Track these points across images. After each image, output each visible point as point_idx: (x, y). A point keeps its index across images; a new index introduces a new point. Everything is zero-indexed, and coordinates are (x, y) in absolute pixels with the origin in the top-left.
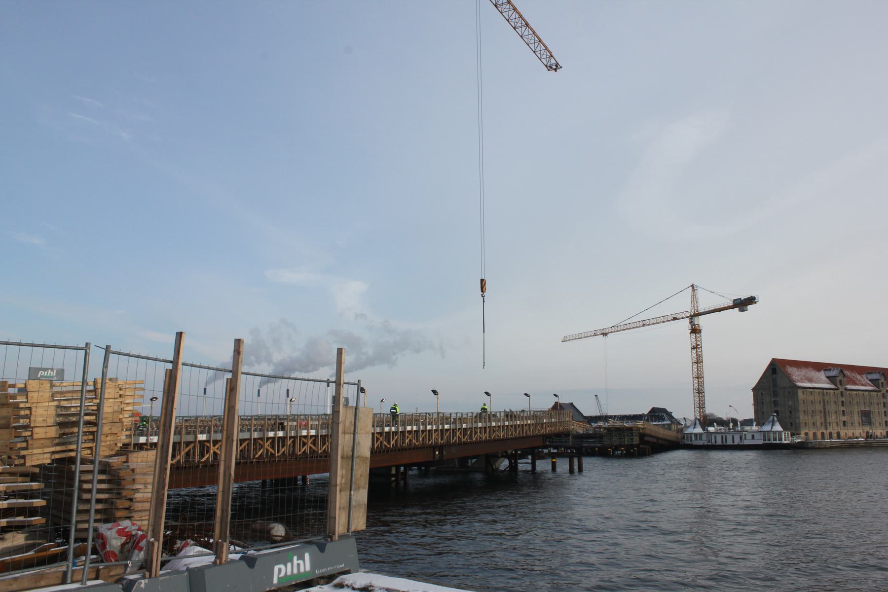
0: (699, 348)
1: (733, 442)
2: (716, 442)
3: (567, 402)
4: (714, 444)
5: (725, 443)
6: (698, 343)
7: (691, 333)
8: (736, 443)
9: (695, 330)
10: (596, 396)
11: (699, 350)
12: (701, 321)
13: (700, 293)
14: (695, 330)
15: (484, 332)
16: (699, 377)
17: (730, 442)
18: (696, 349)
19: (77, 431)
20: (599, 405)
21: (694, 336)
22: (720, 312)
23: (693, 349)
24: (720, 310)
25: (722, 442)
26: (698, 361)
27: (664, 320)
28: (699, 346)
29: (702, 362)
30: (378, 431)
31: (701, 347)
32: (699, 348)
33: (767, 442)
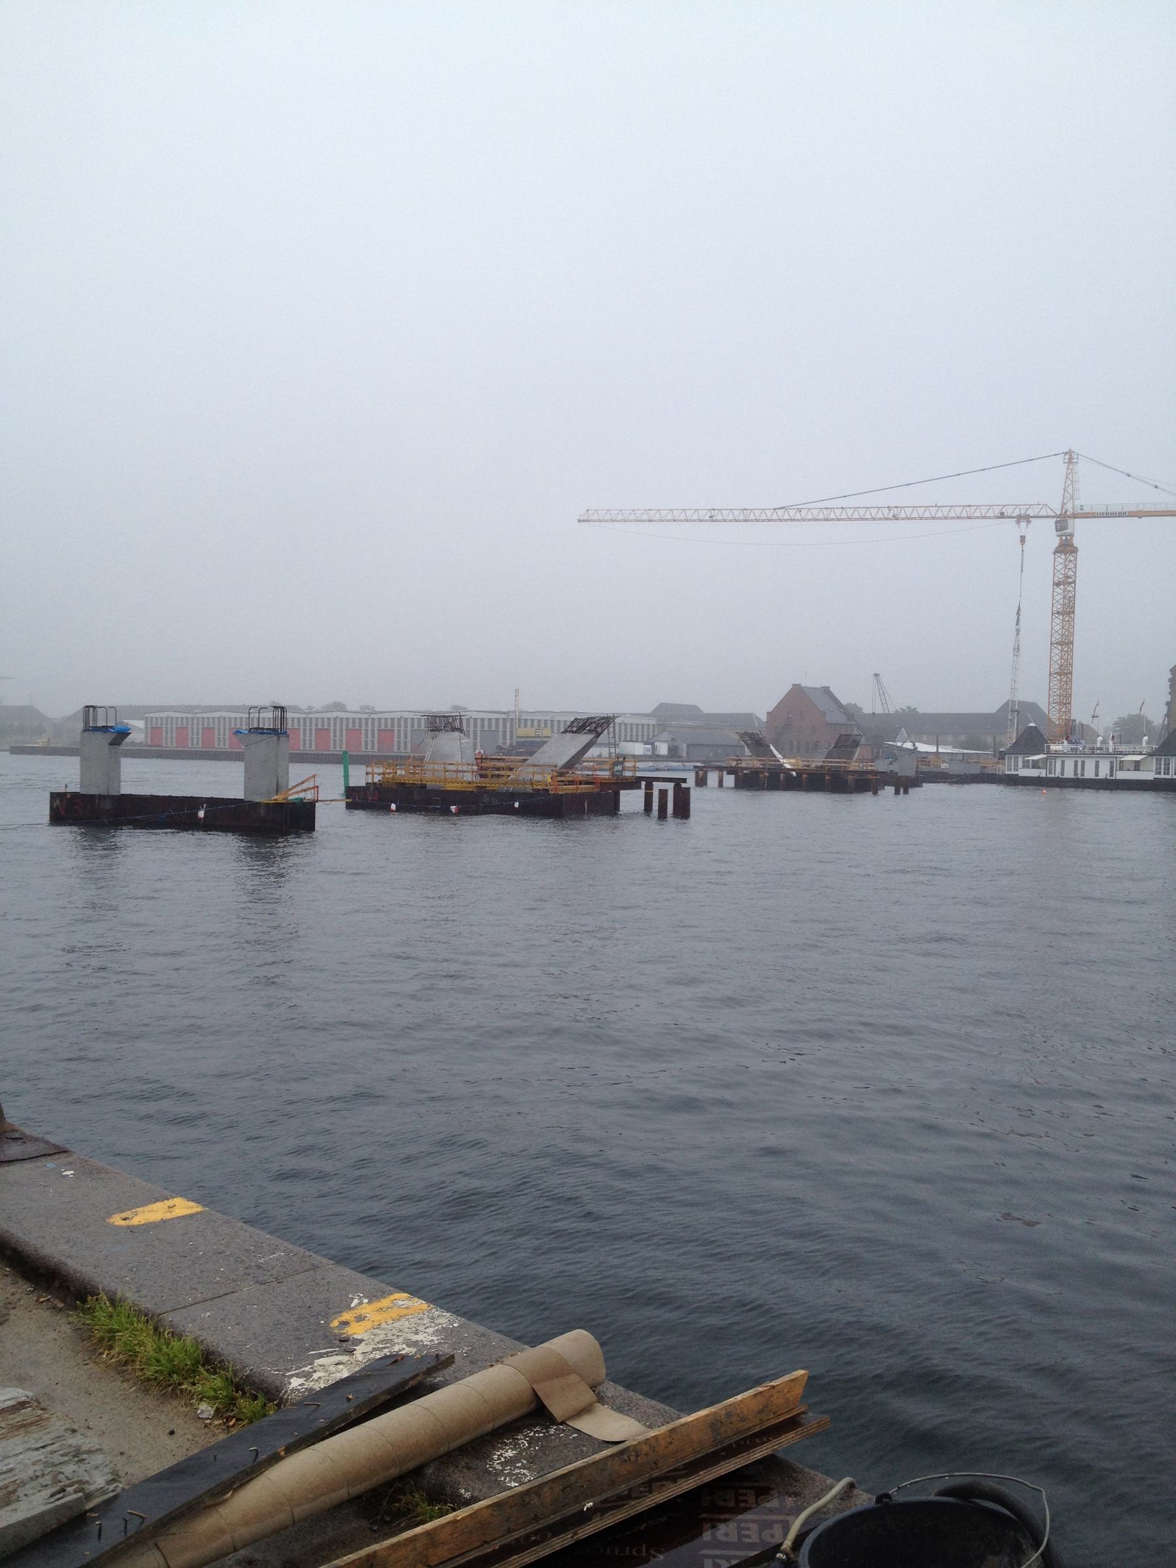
0: (1070, 583)
1: (1097, 775)
2: (1062, 774)
3: (818, 686)
4: (1060, 776)
5: (1079, 776)
6: (1070, 573)
7: (1057, 551)
8: (1102, 776)
9: (1066, 548)
10: (876, 675)
11: (1070, 588)
12: (1081, 531)
13: (1082, 468)
14: (1066, 548)
15: (1019, 607)
16: (1065, 643)
17: (1089, 774)
18: (1064, 585)
19: (664, 733)
20: (882, 694)
21: (1061, 559)
22: (1140, 517)
23: (1057, 584)
24: (1140, 514)
25: (1076, 774)
26: (1067, 611)
27: (967, 513)
28: (1070, 580)
29: (1073, 612)
30: (1051, 747)
31: (1074, 582)
32: (1070, 583)
33: (1162, 776)
